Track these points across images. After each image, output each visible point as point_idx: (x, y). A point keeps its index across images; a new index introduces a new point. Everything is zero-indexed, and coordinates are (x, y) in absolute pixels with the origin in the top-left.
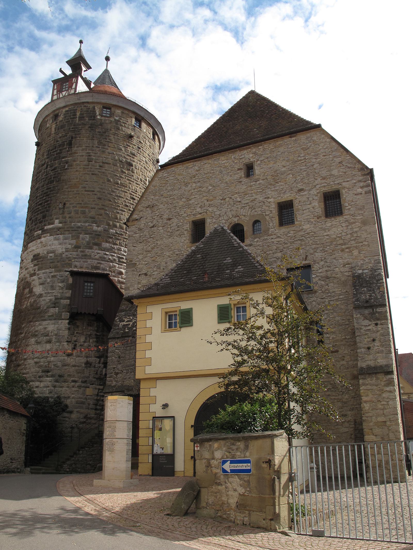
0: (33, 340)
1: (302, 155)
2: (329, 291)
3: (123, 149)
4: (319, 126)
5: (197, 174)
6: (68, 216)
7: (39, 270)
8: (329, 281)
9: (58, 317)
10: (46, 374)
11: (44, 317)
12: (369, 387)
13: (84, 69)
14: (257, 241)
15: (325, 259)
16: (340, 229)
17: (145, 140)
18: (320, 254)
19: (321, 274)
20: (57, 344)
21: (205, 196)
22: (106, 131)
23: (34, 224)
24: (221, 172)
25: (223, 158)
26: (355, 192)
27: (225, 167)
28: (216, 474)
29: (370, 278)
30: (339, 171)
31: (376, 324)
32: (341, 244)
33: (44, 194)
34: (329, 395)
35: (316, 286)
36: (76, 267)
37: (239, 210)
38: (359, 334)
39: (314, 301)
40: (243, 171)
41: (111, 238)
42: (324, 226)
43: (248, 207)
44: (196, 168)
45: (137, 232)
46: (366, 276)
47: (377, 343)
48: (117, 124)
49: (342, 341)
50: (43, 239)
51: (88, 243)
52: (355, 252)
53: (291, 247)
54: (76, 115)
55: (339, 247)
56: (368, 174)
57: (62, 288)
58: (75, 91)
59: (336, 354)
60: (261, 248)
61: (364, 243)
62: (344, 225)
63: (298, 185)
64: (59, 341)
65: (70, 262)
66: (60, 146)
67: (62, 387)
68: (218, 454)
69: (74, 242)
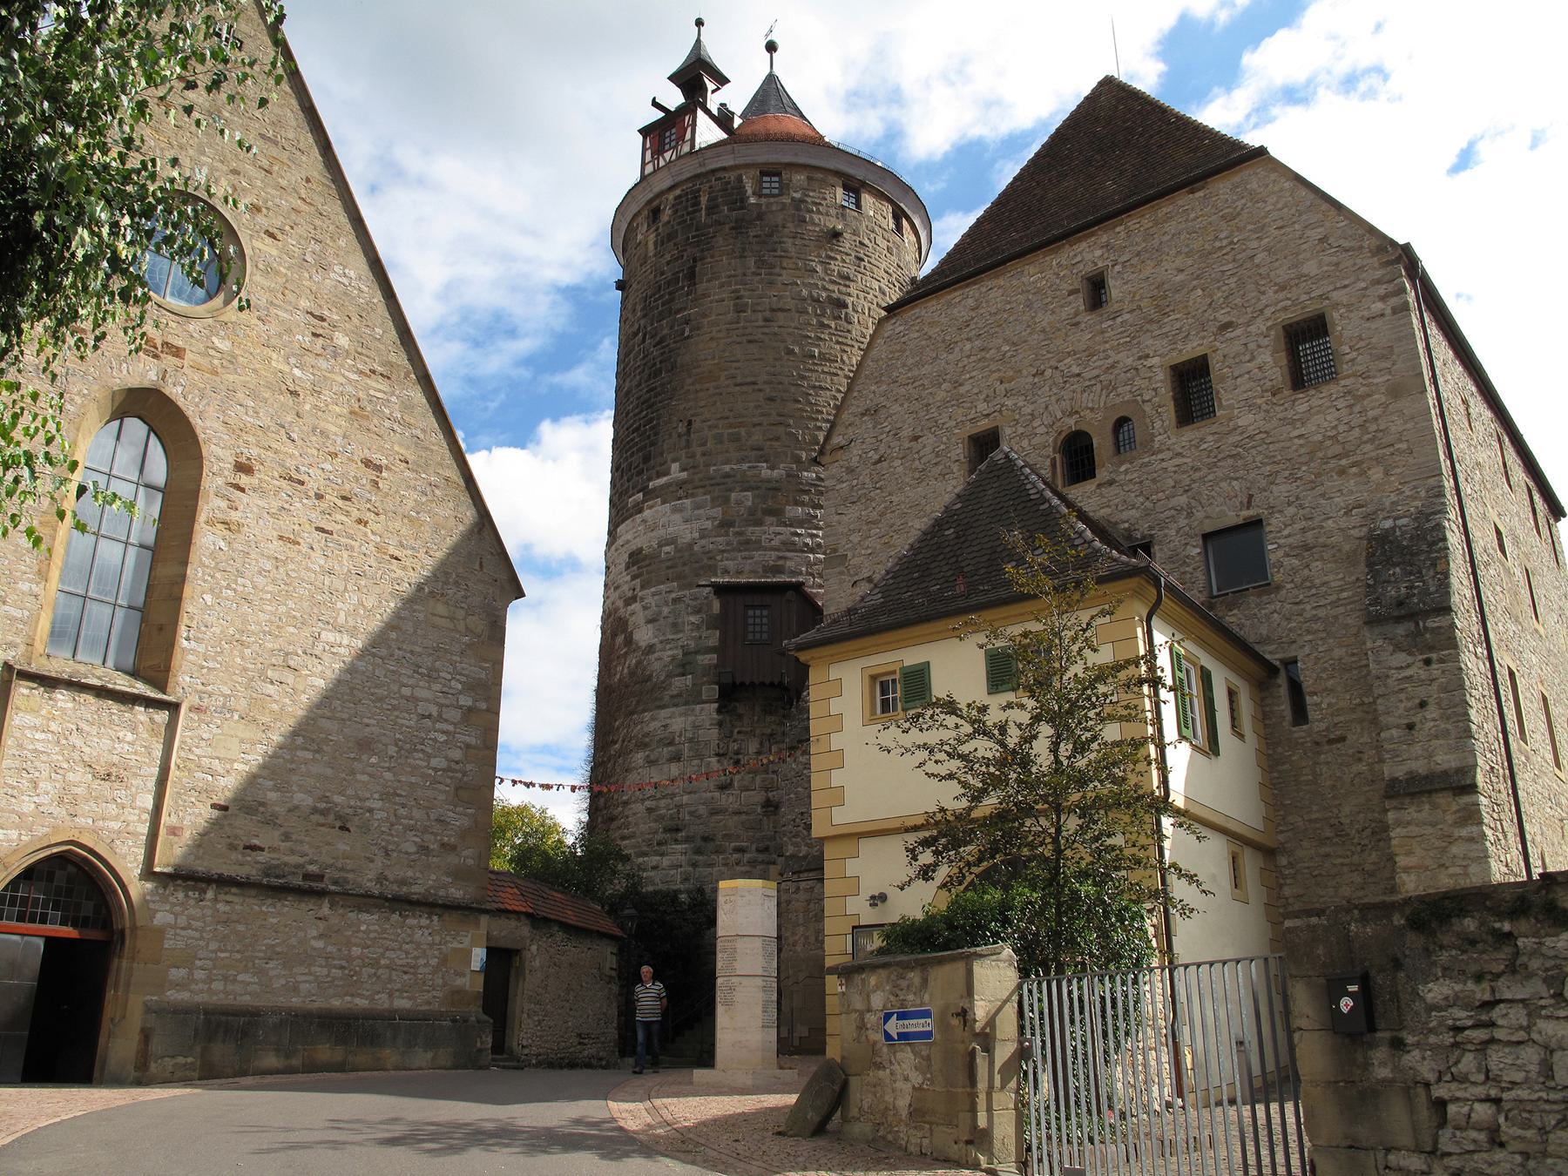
0: (639, 757)
1: (1222, 236)
3: (819, 269)
4: (1261, 152)
6: (699, 450)
7: (643, 587)
9: (691, 698)
12: (1414, 830)
13: (711, 86)
14: (1126, 472)
15: (1298, 498)
16: (1332, 416)
18: (1283, 488)
19: (1291, 540)
24: (1029, 305)
26: (1366, 313)
27: (1038, 291)
28: (875, 1043)
29: (1412, 538)
30: (1320, 263)
31: (1428, 662)
32: (1338, 456)
34: (1327, 855)
38: (1381, 691)
41: (807, 492)
42: (1290, 414)
43: (1099, 386)
44: (971, 302)
46: (1403, 533)
47: (1432, 712)
48: (799, 209)
49: (1353, 710)
50: (647, 513)
51: (752, 511)
52: (1376, 474)
53: (1210, 477)
54: (699, 203)
55: (1333, 463)
56: (1398, 260)
57: (698, 627)
58: (693, 146)
62: (1341, 404)
64: (700, 756)
66: (669, 283)
67: (711, 865)
68: (877, 1000)
69: (717, 512)
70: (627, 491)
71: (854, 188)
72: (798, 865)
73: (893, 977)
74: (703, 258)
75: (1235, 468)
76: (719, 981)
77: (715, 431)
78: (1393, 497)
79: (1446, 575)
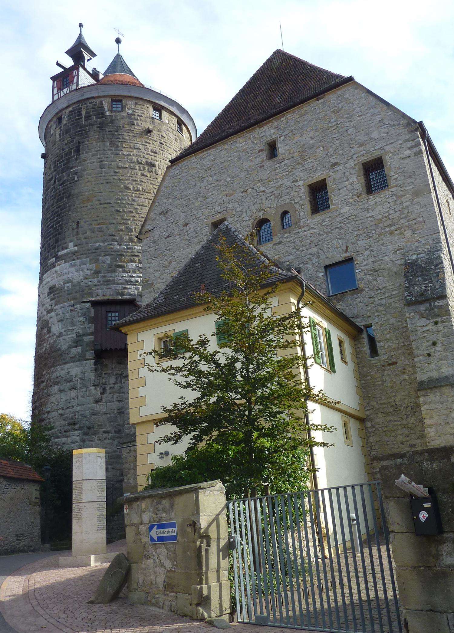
0: (55, 389)
2: (378, 287)
4: (351, 79)
5: (213, 165)
6: (83, 236)
7: (56, 304)
8: (378, 274)
9: (82, 358)
10: (73, 427)
11: (65, 359)
12: (433, 406)
14: (287, 237)
15: (370, 247)
17: (167, 133)
18: (363, 242)
19: (367, 267)
20: (84, 390)
21: (224, 191)
22: (118, 128)
23: (47, 251)
24: (240, 158)
25: (240, 140)
26: (402, 156)
27: (244, 151)
29: (426, 263)
31: (436, 323)
33: (55, 214)
34: (390, 421)
35: (361, 283)
36: (98, 295)
37: (264, 201)
39: (360, 302)
40: (264, 152)
42: (366, 206)
43: (273, 196)
45: (152, 246)
46: (422, 261)
47: (439, 347)
48: (130, 118)
49: (400, 349)
50: (57, 268)
51: (110, 266)
53: (328, 238)
54: (81, 115)
55: (387, 229)
56: (417, 130)
57: (84, 323)
58: (77, 86)
59: (394, 366)
60: (292, 244)
61: (418, 220)
62: (390, 200)
63: (330, 159)
64: (85, 387)
65: (90, 291)
66: (66, 155)
68: (146, 517)
69: (93, 266)
70: (47, 257)
71: (158, 108)
72: (120, 439)
73: (155, 503)
74: (83, 142)
75: (340, 234)
76: (74, 506)
77: (90, 227)
78: (416, 244)
79: (444, 280)
